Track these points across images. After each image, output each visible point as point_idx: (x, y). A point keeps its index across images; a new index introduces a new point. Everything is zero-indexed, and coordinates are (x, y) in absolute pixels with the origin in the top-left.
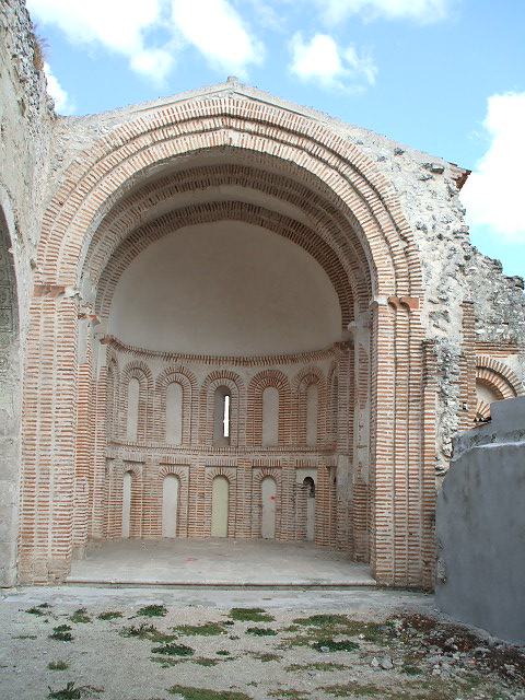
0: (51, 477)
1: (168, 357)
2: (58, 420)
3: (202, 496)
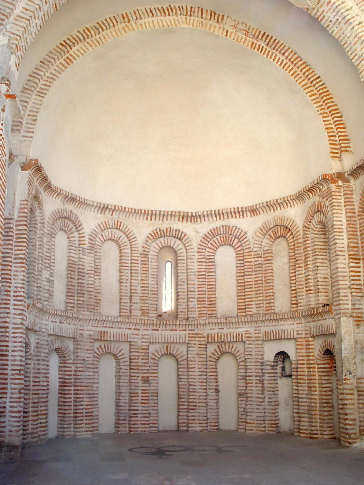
1: (104, 208)
3: (146, 380)
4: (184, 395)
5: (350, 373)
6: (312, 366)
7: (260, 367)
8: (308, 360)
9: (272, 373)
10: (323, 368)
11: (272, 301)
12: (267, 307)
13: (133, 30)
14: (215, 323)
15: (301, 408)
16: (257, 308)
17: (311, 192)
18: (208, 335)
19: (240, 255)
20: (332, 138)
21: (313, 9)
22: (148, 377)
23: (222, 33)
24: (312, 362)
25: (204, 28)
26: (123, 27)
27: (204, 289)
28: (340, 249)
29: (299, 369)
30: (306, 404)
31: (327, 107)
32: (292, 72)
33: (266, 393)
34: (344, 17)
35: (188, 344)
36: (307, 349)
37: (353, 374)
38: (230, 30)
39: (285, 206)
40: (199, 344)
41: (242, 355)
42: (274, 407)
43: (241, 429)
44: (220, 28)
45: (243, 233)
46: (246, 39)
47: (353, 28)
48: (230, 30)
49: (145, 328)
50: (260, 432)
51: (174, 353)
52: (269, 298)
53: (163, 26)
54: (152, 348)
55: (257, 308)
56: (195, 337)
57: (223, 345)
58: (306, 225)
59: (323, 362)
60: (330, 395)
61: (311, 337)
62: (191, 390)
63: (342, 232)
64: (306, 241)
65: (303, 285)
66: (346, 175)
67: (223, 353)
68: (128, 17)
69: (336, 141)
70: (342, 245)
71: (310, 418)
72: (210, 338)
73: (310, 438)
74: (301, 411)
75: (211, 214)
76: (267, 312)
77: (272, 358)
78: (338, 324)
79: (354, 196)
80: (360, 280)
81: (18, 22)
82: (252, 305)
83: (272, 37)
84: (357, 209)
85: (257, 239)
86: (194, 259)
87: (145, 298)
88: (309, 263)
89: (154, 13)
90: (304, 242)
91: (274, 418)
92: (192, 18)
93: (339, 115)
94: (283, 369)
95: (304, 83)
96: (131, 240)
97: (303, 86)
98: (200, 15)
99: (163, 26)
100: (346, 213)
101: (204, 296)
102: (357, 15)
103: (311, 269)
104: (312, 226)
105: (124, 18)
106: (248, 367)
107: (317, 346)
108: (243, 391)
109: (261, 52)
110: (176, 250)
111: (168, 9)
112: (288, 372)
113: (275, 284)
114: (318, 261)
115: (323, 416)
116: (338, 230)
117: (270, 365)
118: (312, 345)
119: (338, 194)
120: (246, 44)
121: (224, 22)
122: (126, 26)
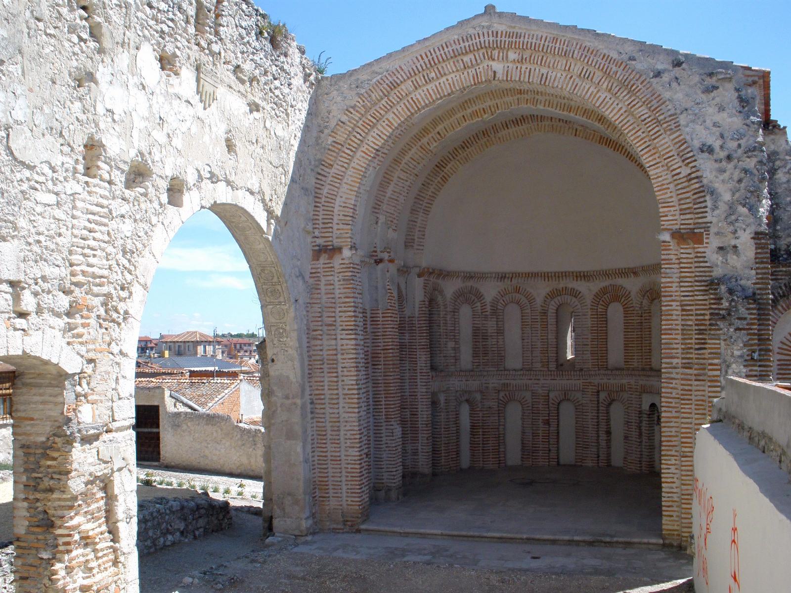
0: (342, 433)
1: (502, 277)
2: (345, 378)
3: (547, 423)
44: (569, 128)
54: (552, 395)
77: (648, 408)
81: (390, 203)
96: (531, 300)
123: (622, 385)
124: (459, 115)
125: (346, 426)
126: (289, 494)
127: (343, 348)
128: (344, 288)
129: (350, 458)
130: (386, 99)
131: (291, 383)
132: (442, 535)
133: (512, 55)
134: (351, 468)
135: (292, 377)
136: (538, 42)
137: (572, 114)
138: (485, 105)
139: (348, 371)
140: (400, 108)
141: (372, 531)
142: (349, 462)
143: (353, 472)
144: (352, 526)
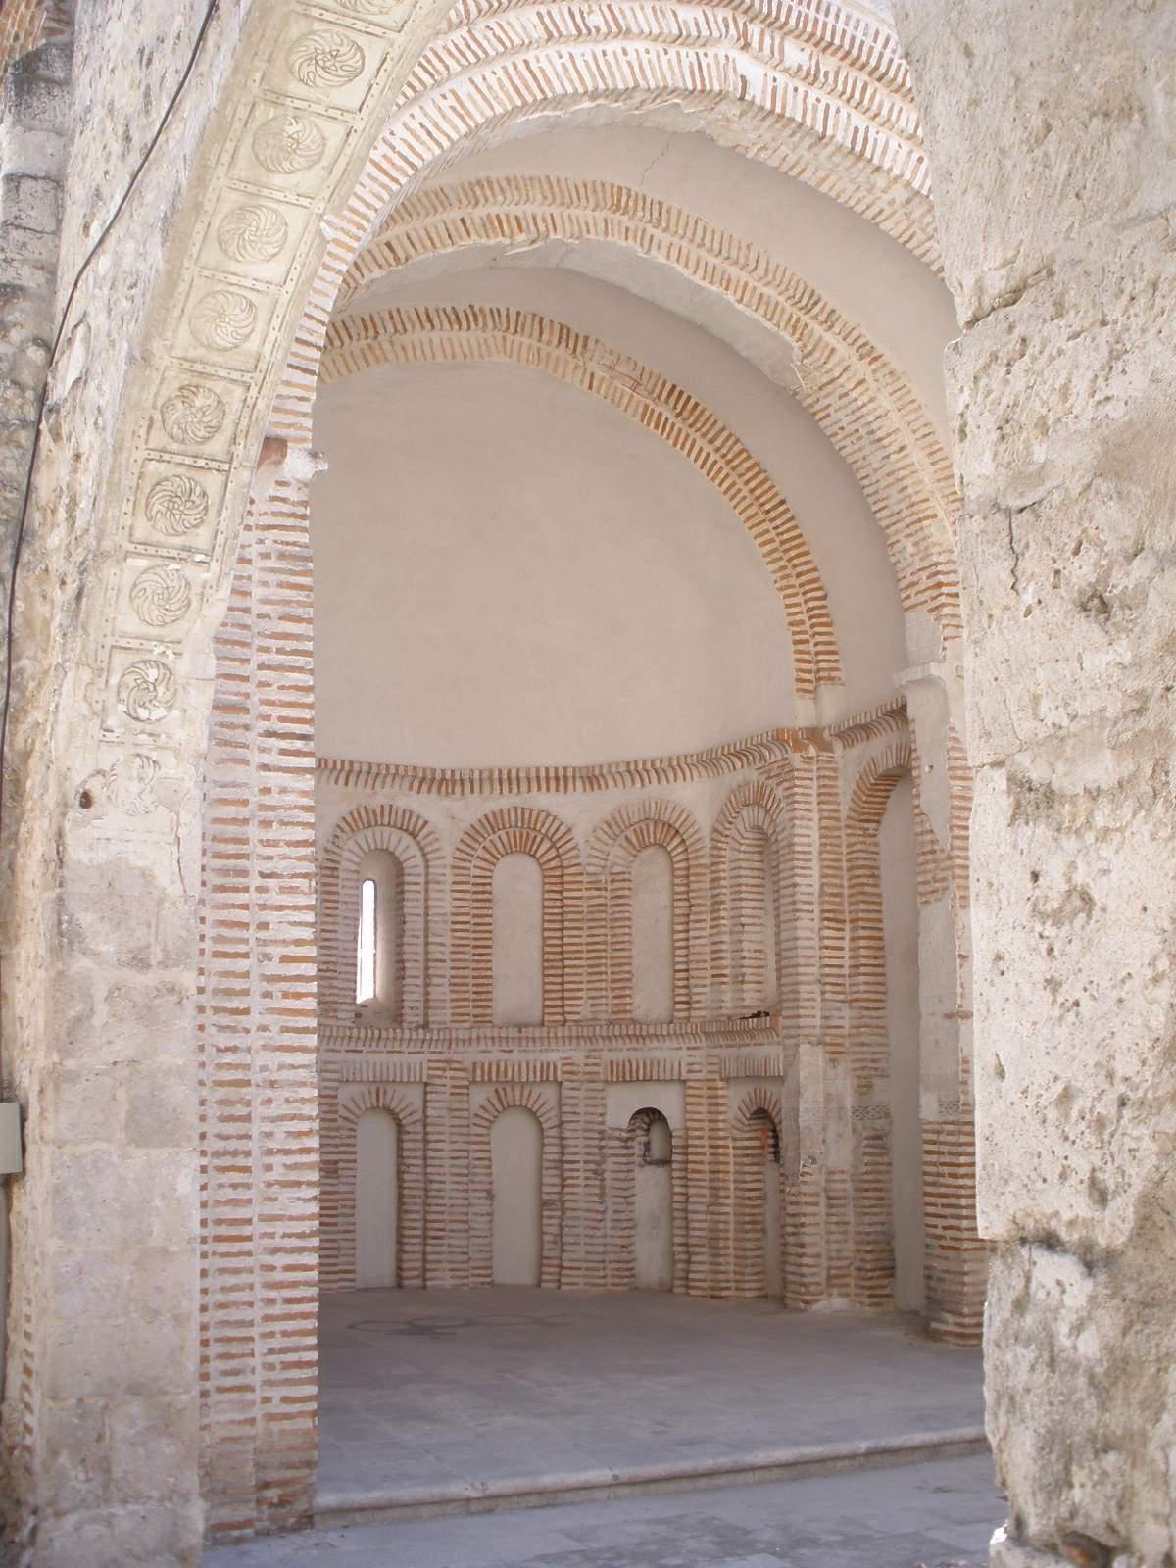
2: (271, 917)
4: (415, 1204)
5: (814, 1161)
6: (721, 1142)
7: (596, 1142)
8: (711, 1130)
9: (624, 1156)
10: (747, 1148)
11: (628, 992)
12: (617, 1005)
13: (386, 359)
14: (493, 1038)
15: (692, 1233)
16: (593, 1005)
17: (740, 759)
18: (475, 1064)
19: (553, 880)
20: (801, 647)
21: (809, 396)
22: (336, 1162)
23: (582, 381)
24: (721, 1134)
25: (542, 366)
26: (362, 350)
27: (467, 957)
28: (805, 898)
29: (690, 1150)
30: (704, 1225)
31: (794, 573)
32: (726, 484)
33: (609, 1200)
34: (872, 432)
35: (426, 1084)
36: (710, 1105)
37: (820, 1162)
38: (600, 373)
39: (671, 776)
40: (454, 1087)
41: (553, 1113)
42: (625, 1233)
43: (547, 1281)
44: (577, 367)
45: (563, 829)
46: (632, 397)
47: (888, 456)
48: (600, 373)
49: (331, 1046)
50: (595, 1288)
51: (393, 1106)
52: (622, 985)
53: (453, 357)
55: (593, 1005)
56: (444, 1070)
57: (508, 1089)
58: (721, 828)
59: (747, 1135)
60: (760, 1206)
61: (722, 1080)
62: (434, 1193)
63: (810, 860)
64: (717, 864)
65: (705, 962)
66: (826, 734)
67: (507, 1107)
68: (375, 327)
69: (808, 653)
70: (810, 889)
71: (712, 1255)
72: (479, 1072)
73: (713, 1297)
74: (692, 1241)
75: (491, 779)
76: (614, 1017)
77: (625, 1123)
78: (792, 1059)
79: (840, 782)
80: (841, 967)
82: (580, 998)
83: (689, 398)
84: (844, 813)
85: (598, 845)
86: (444, 883)
87: (329, 974)
88: (723, 914)
89: (436, 322)
90: (713, 864)
91: (625, 1256)
92: (518, 338)
93: (820, 593)
94: (647, 1146)
95: (750, 512)
97: (748, 519)
98: (536, 334)
99: (453, 357)
100: (821, 819)
101: (466, 973)
102: (898, 430)
103: (727, 929)
104: (733, 832)
105: (366, 329)
106: (568, 1142)
107: (735, 1100)
108: (555, 1197)
109: (662, 433)
110: (402, 859)
111: (466, 314)
112: (657, 1152)
113: (634, 953)
114: (744, 912)
115: (744, 1249)
116: (800, 856)
117: (619, 1139)
118: (723, 1096)
119: (805, 775)
120: (631, 410)
121: (588, 354)
122: (370, 346)
123: (545, 1067)
124: (453, 215)
125: (269, 1101)
126: (135, 1390)
127: (267, 800)
128: (281, 585)
129: (280, 1228)
130: (463, 32)
131: (160, 901)
132: (617, 1483)
133: (796, 54)
134: (289, 1268)
135: (165, 878)
136: (869, 42)
137: (730, 297)
138: (526, 210)
139: (283, 890)
140: (492, 75)
141: (361, 1509)
142: (278, 1241)
143: (294, 1284)
144: (283, 1503)
